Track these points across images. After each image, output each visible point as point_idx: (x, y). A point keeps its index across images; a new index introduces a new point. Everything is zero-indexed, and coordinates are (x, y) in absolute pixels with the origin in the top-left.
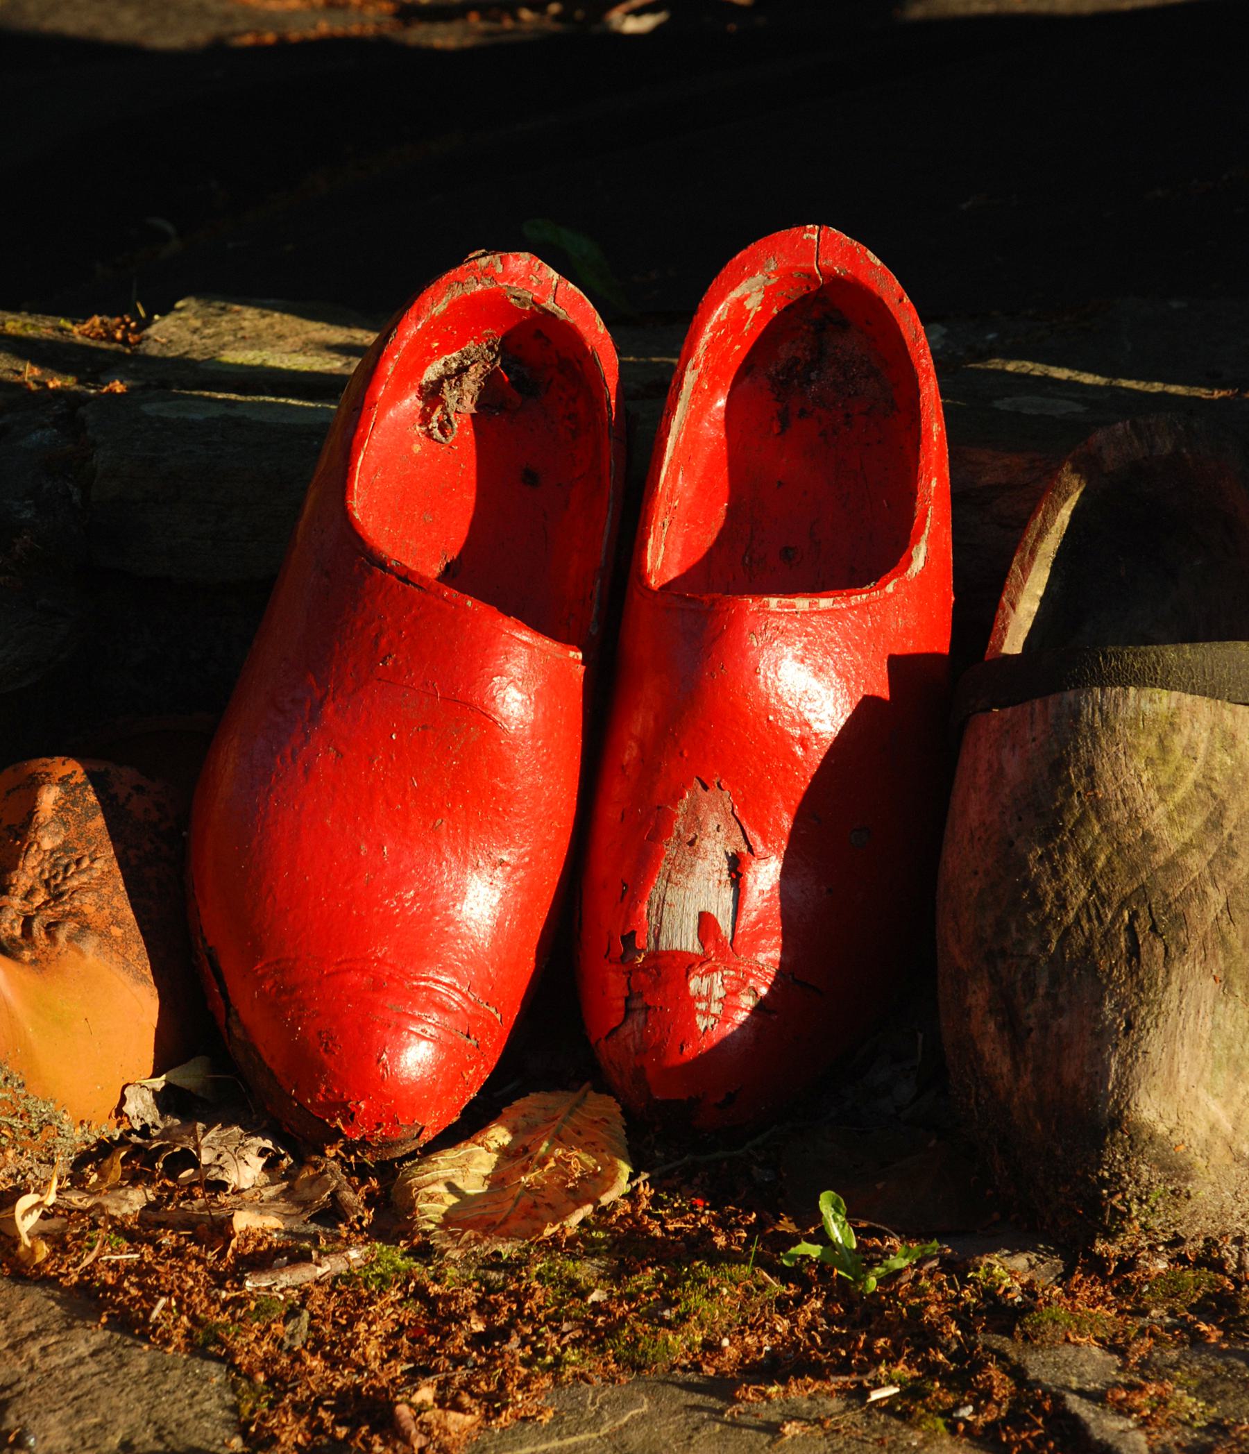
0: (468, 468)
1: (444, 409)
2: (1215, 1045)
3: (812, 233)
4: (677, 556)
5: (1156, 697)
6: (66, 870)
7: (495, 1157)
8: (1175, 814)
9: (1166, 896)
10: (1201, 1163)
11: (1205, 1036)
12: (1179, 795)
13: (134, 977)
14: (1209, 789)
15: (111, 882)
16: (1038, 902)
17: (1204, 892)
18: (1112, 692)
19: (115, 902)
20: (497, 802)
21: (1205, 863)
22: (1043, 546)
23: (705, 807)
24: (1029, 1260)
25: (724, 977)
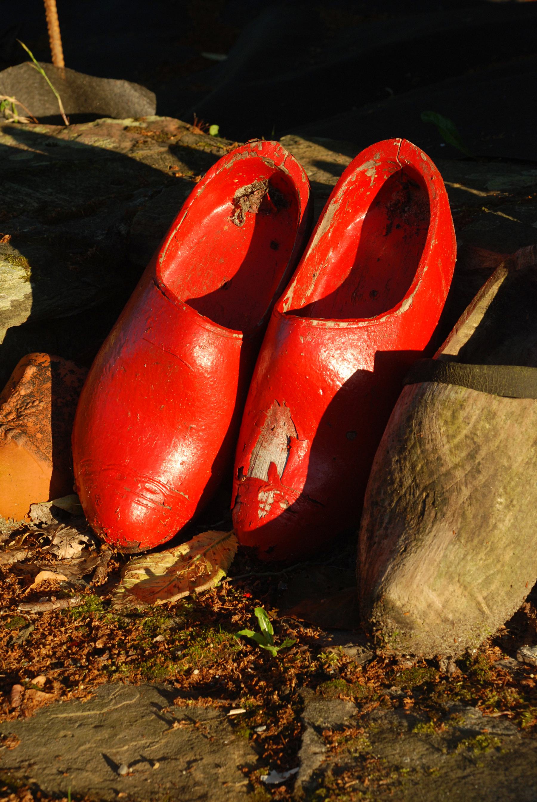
0: (246, 239)
1: (241, 210)
2: (441, 565)
3: (398, 143)
4: (320, 290)
5: (459, 391)
6: (27, 405)
7: (176, 559)
8: (453, 450)
9: (443, 488)
10: (419, 621)
11: (438, 560)
12: (456, 441)
13: (40, 457)
14: (473, 439)
15: (45, 413)
16: (392, 482)
17: (460, 489)
18: (442, 385)
19: (44, 422)
20: (188, 400)
21: (463, 475)
22: (480, 303)
23: (279, 414)
24: (358, 650)
25: (274, 494)
